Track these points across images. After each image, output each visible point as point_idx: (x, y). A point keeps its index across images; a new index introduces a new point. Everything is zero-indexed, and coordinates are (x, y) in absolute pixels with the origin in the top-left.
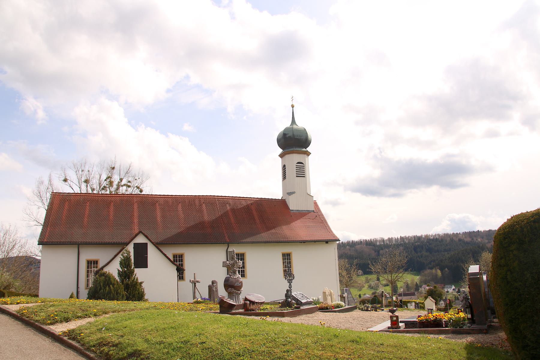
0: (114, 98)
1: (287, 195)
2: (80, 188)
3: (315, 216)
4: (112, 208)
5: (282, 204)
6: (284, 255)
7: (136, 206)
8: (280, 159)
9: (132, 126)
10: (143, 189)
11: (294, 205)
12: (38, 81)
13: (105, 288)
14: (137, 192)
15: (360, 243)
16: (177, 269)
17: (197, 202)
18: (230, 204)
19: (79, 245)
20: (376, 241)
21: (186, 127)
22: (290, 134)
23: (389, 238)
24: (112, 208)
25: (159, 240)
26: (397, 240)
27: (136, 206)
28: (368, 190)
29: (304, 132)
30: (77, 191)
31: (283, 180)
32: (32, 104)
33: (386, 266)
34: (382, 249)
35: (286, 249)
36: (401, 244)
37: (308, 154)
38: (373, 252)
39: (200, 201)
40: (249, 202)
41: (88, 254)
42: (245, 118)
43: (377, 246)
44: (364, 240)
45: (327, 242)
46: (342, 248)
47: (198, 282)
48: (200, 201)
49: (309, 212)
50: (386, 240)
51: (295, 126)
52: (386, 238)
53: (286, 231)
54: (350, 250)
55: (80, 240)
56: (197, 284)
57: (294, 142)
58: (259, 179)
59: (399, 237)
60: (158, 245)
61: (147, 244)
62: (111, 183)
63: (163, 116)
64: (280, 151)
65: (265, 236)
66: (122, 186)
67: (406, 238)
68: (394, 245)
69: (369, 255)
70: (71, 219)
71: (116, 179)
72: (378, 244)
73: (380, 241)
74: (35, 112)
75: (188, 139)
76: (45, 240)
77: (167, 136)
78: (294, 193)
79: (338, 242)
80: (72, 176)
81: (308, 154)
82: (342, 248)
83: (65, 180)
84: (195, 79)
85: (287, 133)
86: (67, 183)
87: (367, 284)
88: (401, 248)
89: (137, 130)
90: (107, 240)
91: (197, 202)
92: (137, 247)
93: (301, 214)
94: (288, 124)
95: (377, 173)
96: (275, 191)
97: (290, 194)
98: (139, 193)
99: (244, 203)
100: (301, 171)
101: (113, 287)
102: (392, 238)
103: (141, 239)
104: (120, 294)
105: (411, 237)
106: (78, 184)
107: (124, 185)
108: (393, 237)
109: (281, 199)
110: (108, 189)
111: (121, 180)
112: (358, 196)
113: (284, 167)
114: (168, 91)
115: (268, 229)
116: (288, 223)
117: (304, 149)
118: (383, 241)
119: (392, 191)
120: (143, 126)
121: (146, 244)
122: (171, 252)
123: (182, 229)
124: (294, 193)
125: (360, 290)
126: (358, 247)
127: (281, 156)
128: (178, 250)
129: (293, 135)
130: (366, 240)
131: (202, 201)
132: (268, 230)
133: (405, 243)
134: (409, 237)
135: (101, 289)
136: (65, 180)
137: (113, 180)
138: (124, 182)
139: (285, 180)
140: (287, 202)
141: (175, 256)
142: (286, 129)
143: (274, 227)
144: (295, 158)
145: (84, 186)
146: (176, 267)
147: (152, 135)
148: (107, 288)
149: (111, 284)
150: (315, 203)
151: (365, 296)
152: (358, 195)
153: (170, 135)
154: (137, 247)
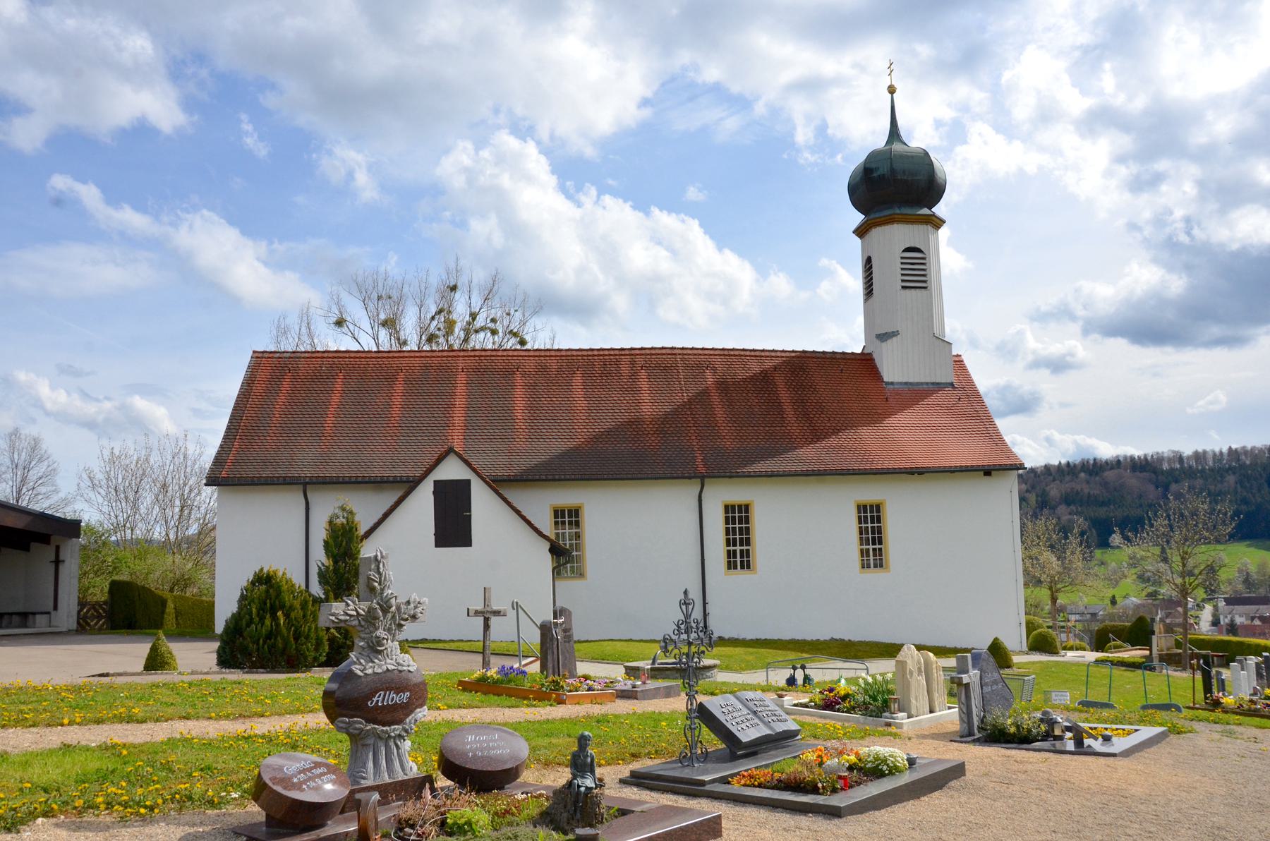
0: (523, 130)
1: (878, 342)
2: (376, 339)
3: (956, 395)
4: (399, 387)
5: (864, 364)
6: (862, 508)
7: (461, 381)
8: (858, 240)
9: (569, 196)
10: (527, 338)
11: (895, 368)
12: (357, 103)
13: (262, 619)
14: (511, 343)
15: (1117, 464)
16: (551, 550)
17: (625, 366)
18: (714, 369)
19: (306, 485)
20: (1160, 459)
21: (693, 194)
22: (884, 169)
23: (1196, 453)
24: (399, 387)
25: (501, 472)
26: (1218, 457)
27: (461, 381)
28: (1148, 327)
29: (923, 162)
30: (368, 344)
31: (866, 300)
32: (352, 161)
33: (1168, 542)
34: (1176, 482)
35: (870, 492)
36: (1230, 468)
37: (937, 223)
38: (1151, 488)
39: (633, 363)
40: (769, 363)
41: (326, 507)
42: (839, 157)
43: (1162, 472)
44: (1125, 457)
45: (987, 472)
46: (1068, 478)
47: (497, 613)
48: (633, 363)
49: (938, 386)
50: (1188, 458)
51: (897, 147)
52: (1187, 451)
53: (870, 442)
54: (1088, 482)
55: (308, 473)
56: (494, 620)
57: (896, 190)
58: (797, 296)
59: (1225, 450)
60: (497, 484)
61: (436, 482)
62: (450, 325)
63: (632, 167)
64: (858, 218)
65: (807, 456)
66: (477, 331)
67: (1245, 451)
68: (1212, 470)
69: (1140, 497)
70: (296, 416)
71: (460, 312)
72: (1165, 466)
73: (1169, 460)
74: (350, 175)
75: (696, 222)
76: (224, 474)
77: (647, 214)
78: (894, 334)
79: (1021, 471)
80: (357, 312)
81: (937, 223)
82: (1068, 478)
83: (340, 323)
84: (712, 73)
85: (873, 166)
86: (345, 329)
87: (1134, 571)
88: (1231, 479)
89: (579, 205)
90: (376, 473)
91: (625, 366)
92: (442, 489)
93: (915, 394)
94: (880, 142)
95: (1177, 285)
96: (845, 333)
97: (883, 337)
98: (519, 347)
99: (755, 367)
100: (917, 271)
101: (287, 616)
102: (1205, 452)
103: (451, 470)
104: (307, 637)
105: (1261, 450)
106: (370, 331)
107: (483, 329)
108: (1208, 448)
109: (862, 354)
110: (441, 340)
111: (474, 316)
112: (1120, 345)
113: (868, 263)
114: (645, 103)
115: (817, 435)
116: (875, 417)
117: (925, 211)
118: (1181, 459)
119: (1216, 330)
120: (593, 192)
121: (467, 483)
122: (541, 504)
123: (580, 440)
124: (894, 334)
125: (1115, 583)
126: (1109, 475)
127: (861, 232)
128: (566, 497)
129: (893, 170)
130: (1132, 458)
131: (640, 362)
132: (819, 440)
133: (1243, 466)
134: (1253, 449)
135: (251, 622)
136: (340, 323)
137: (454, 316)
138: (480, 321)
139: (871, 300)
140: (877, 362)
141: (558, 513)
142: (874, 156)
143: (836, 432)
144: (897, 236)
145: (383, 334)
146: (548, 545)
147: (617, 215)
148: (268, 622)
149: (282, 607)
150: (958, 362)
151: (1127, 601)
152: (1121, 344)
153: (656, 211)
154: (442, 489)
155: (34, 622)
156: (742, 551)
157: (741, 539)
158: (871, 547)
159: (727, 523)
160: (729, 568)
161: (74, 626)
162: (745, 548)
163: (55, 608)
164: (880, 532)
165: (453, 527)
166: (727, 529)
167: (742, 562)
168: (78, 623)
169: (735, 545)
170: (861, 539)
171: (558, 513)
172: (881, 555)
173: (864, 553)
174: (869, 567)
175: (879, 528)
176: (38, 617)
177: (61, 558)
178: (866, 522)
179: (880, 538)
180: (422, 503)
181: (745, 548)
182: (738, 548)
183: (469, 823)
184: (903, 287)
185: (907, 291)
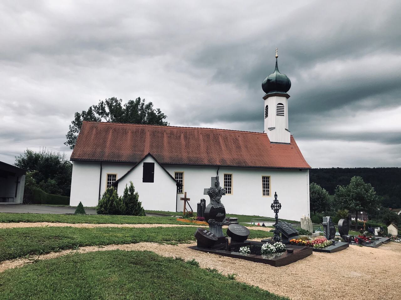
6: (263, 178)
17: (196, 133)
41: (108, 171)
64: (264, 94)
103: (149, 160)
155: (8, 200)
156: (229, 188)
157: (229, 185)
158: (266, 189)
159: (225, 180)
160: (264, 194)
161: (22, 202)
162: (268, 189)
163: (16, 197)
164: (268, 185)
165: (148, 177)
166: (225, 181)
167: (229, 191)
168: (23, 201)
169: (227, 186)
170: (263, 187)
171: (176, 174)
172: (269, 192)
173: (264, 191)
174: (265, 195)
175: (268, 184)
176: (9, 199)
177: (19, 181)
178: (227, 180)
179: (269, 187)
180: (139, 171)
181: (268, 189)
182: (228, 187)
183: (370, 219)
184: (277, 115)
185: (278, 116)
